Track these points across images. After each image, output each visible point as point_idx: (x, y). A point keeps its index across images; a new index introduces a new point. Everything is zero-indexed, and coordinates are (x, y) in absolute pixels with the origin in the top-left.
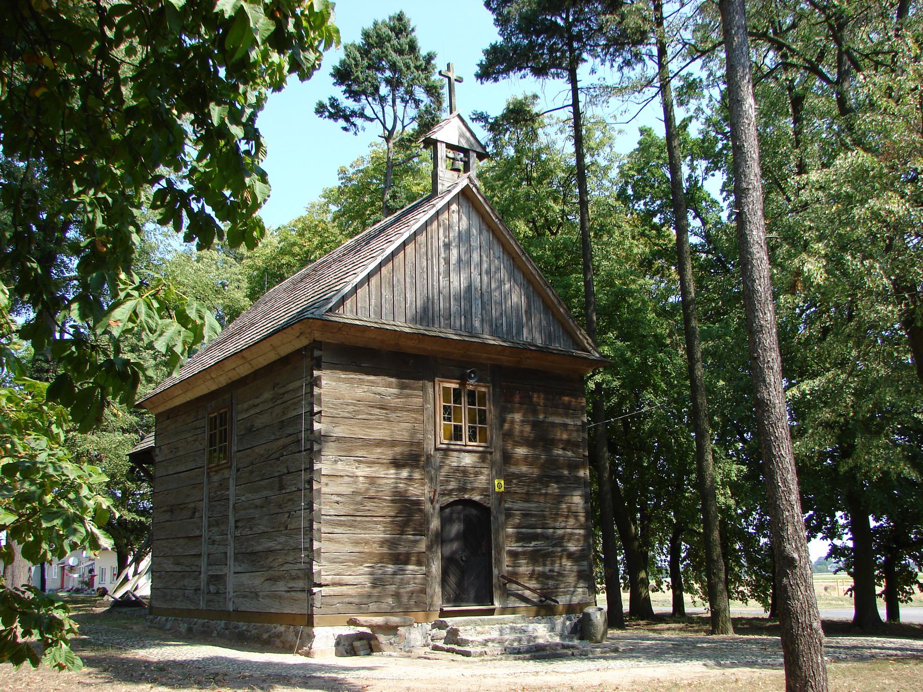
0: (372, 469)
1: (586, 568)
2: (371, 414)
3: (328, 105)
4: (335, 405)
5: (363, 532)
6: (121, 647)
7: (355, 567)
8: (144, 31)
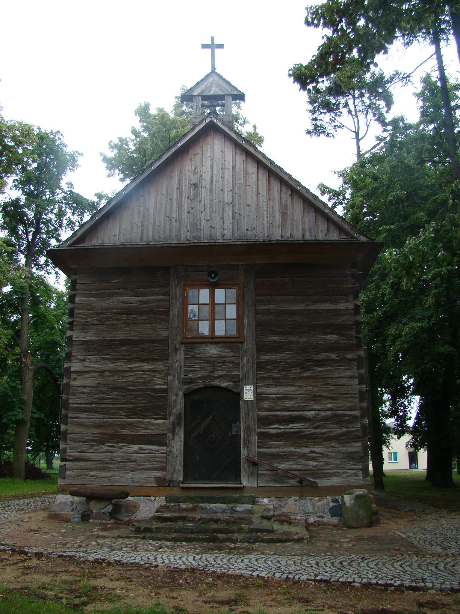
0: (117, 364)
1: (359, 449)
2: (117, 320)
3: (141, 130)
4: (86, 315)
5: (106, 416)
6: (372, 460)
7: (97, 446)
8: (450, 408)
